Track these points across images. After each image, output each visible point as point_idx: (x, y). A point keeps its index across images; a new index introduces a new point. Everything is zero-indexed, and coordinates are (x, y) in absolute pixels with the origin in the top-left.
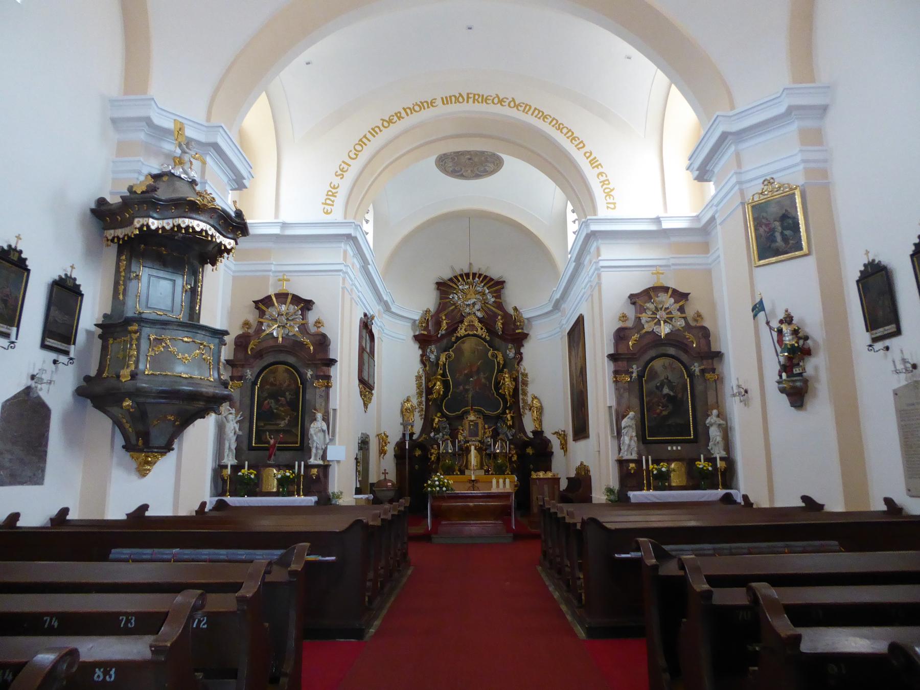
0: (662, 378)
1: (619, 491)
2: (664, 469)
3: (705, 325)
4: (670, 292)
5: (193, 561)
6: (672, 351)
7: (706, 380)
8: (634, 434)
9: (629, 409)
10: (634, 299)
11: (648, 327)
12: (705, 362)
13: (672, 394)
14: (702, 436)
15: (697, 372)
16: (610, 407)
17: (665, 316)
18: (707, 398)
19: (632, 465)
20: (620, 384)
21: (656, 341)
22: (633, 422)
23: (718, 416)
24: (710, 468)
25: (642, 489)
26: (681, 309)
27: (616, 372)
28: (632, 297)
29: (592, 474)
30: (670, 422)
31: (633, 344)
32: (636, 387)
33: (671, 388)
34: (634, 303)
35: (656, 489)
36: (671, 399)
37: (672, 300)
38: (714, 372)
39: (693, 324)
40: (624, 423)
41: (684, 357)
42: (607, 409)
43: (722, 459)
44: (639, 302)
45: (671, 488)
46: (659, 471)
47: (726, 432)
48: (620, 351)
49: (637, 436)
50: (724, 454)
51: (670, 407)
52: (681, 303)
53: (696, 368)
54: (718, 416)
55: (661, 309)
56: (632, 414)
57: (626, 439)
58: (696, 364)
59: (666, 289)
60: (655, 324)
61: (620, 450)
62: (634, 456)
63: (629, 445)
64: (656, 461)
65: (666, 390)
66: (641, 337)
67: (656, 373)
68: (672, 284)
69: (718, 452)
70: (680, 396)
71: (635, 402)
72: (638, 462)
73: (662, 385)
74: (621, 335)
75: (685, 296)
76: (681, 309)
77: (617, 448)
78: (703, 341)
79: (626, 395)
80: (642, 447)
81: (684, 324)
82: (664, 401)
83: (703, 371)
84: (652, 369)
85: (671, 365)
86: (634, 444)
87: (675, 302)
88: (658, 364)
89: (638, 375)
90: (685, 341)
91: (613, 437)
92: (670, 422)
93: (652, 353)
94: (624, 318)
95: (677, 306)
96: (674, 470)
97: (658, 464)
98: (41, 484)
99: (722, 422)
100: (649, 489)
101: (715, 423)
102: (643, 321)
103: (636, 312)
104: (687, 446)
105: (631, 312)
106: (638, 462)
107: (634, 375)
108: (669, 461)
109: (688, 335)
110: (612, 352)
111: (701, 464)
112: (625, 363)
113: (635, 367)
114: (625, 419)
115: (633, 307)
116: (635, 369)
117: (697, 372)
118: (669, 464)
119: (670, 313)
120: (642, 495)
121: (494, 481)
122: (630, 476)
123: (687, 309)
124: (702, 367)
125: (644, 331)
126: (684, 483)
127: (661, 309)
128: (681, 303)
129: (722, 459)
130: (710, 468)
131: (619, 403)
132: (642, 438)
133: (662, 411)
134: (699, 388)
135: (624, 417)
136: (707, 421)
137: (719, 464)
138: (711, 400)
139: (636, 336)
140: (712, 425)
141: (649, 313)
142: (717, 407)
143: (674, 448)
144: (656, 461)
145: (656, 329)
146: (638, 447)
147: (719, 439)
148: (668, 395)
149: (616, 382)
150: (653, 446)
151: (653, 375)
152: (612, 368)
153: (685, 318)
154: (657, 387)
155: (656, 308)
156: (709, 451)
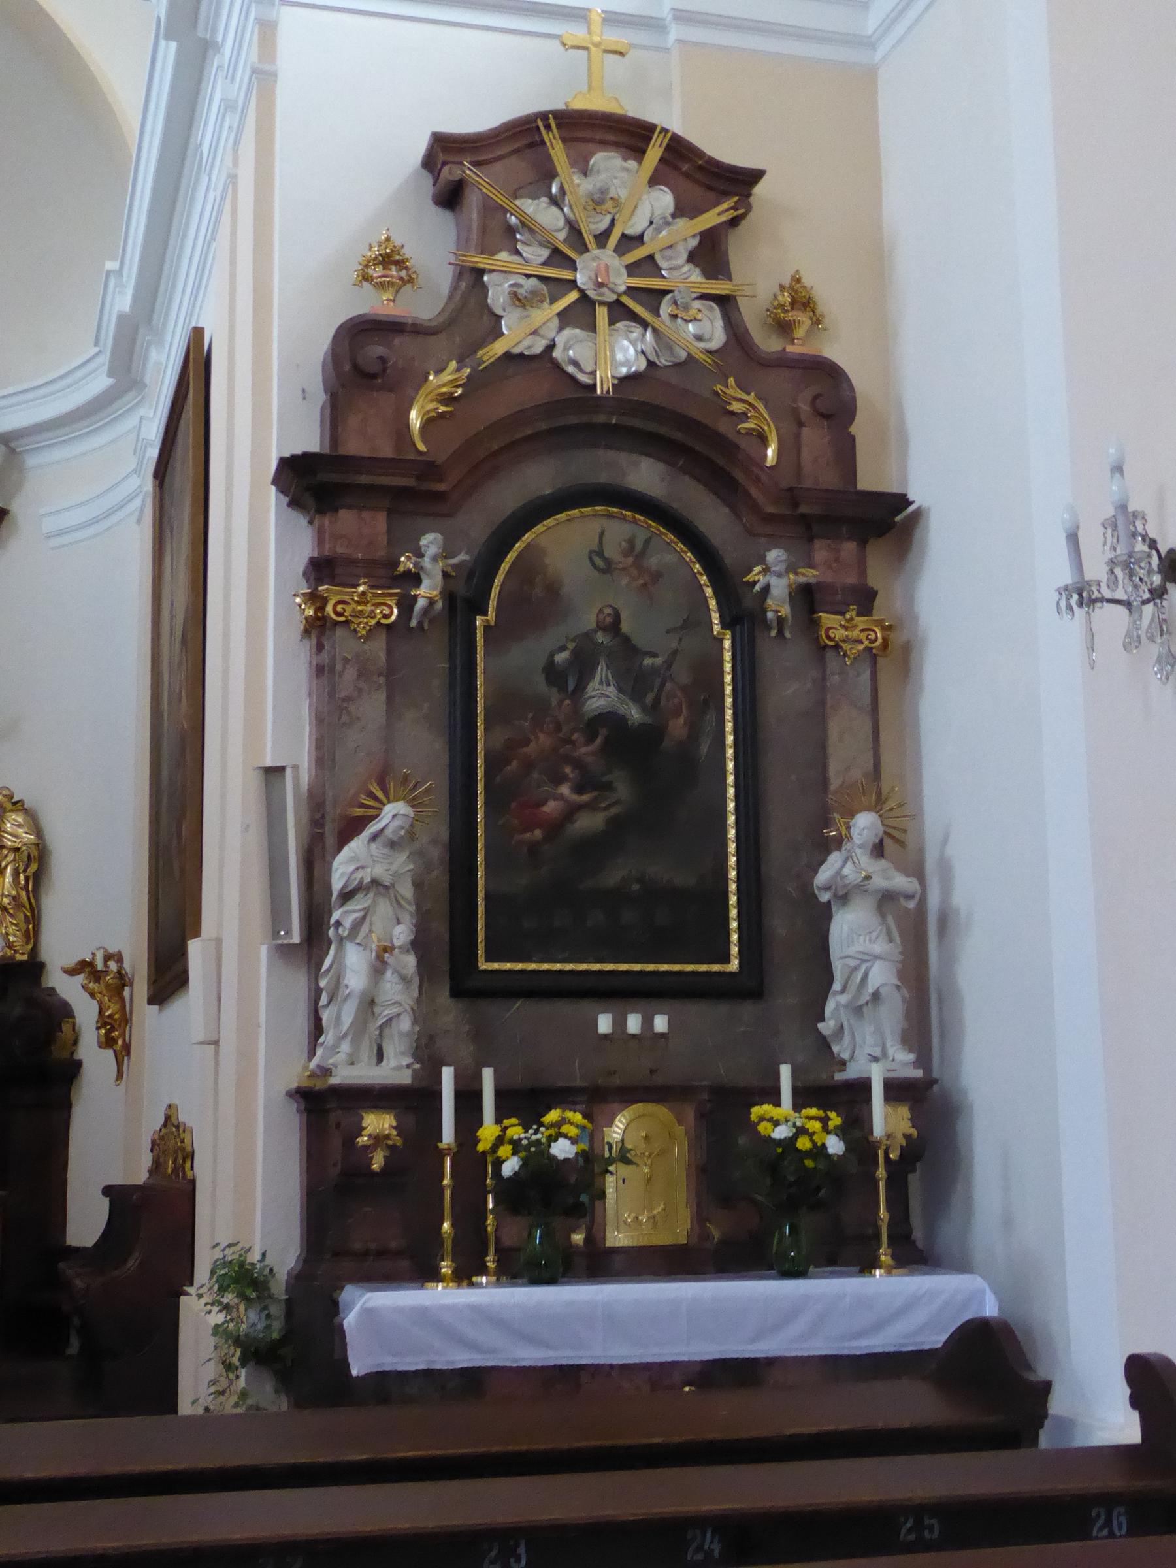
0: (589, 620)
1: (299, 1279)
2: (562, 1149)
3: (833, 352)
4: (654, 153)
6: (646, 475)
7: (822, 650)
8: (402, 934)
9: (386, 779)
10: (453, 167)
11: (518, 333)
12: (821, 551)
13: (634, 714)
14: (785, 965)
15: (779, 603)
16: (273, 773)
17: (622, 281)
18: (824, 768)
19: (378, 1123)
20: (343, 644)
21: (573, 415)
22: (402, 862)
23: (878, 850)
24: (835, 1146)
25: (427, 1274)
26: (710, 254)
27: (322, 569)
28: (444, 149)
29: (202, 1171)
30: (614, 875)
31: (429, 423)
32: (434, 657)
33: (635, 683)
34: (450, 197)
35: (516, 1268)
36: (625, 743)
37: (664, 199)
38: (866, 609)
39: (769, 344)
40: (346, 864)
41: (713, 518)
42: (256, 782)
43: (896, 1090)
44: (483, 183)
45: (599, 1264)
46: (539, 1164)
47: (919, 933)
48: (354, 447)
49: (418, 945)
50: (904, 1062)
51: (623, 790)
52: (712, 218)
53: (775, 577)
54: (878, 850)
55: (602, 239)
56: (394, 814)
57: (354, 965)
58: (774, 555)
59: (631, 135)
60: (565, 318)
61: (317, 1029)
62: (396, 1069)
63: (369, 1003)
64: (523, 1102)
65: (602, 694)
66: (471, 384)
67: (553, 590)
68: (671, 116)
69: (873, 1053)
70: (677, 727)
71: (423, 747)
72: (415, 1102)
74: (364, 361)
75: (737, 182)
76: (710, 254)
77: (301, 1024)
78: (815, 438)
79: (372, 707)
80: (451, 1014)
81: (717, 335)
82: (585, 751)
83: (808, 599)
84: (527, 569)
85: (636, 552)
86: (397, 994)
87: (683, 210)
88: (566, 544)
89: (450, 596)
90: (723, 426)
91: (284, 951)
92: (615, 874)
93: (538, 477)
94: (389, 261)
95: (688, 231)
96: (624, 1157)
97: (531, 1119)
99: (902, 882)
100: (464, 1275)
101: (861, 888)
102: (498, 293)
103: (463, 243)
104: (704, 1015)
105: (433, 247)
106: (415, 1102)
107: (427, 591)
108: (598, 1099)
109: (737, 397)
110: (308, 439)
111: (780, 1120)
112: (378, 523)
113: (430, 542)
114: (357, 846)
115: (444, 218)
116: (432, 557)
117: (779, 603)
118: (596, 1118)
119: (648, 265)
120: (422, 1315)
122: (374, 1193)
123: (737, 249)
124: (809, 575)
125: (498, 348)
126: (678, 1232)
127: (602, 239)
128: (712, 218)
129: (896, 1090)
130: (835, 1146)
131: (324, 756)
132: (451, 960)
133: (572, 811)
134: (785, 693)
135: (351, 828)
136: (824, 875)
137: (886, 1121)
138: (845, 758)
139: (446, 378)
140: (844, 899)
141: (535, 254)
142: (877, 804)
143: (634, 1024)
144: (523, 1102)
145: (572, 347)
146: (422, 1013)
147: (881, 976)
148: (610, 720)
149: (318, 627)
150: (517, 1014)
151: (536, 602)
152: (304, 544)
153: (725, 302)
155: (574, 229)
156: (824, 1044)
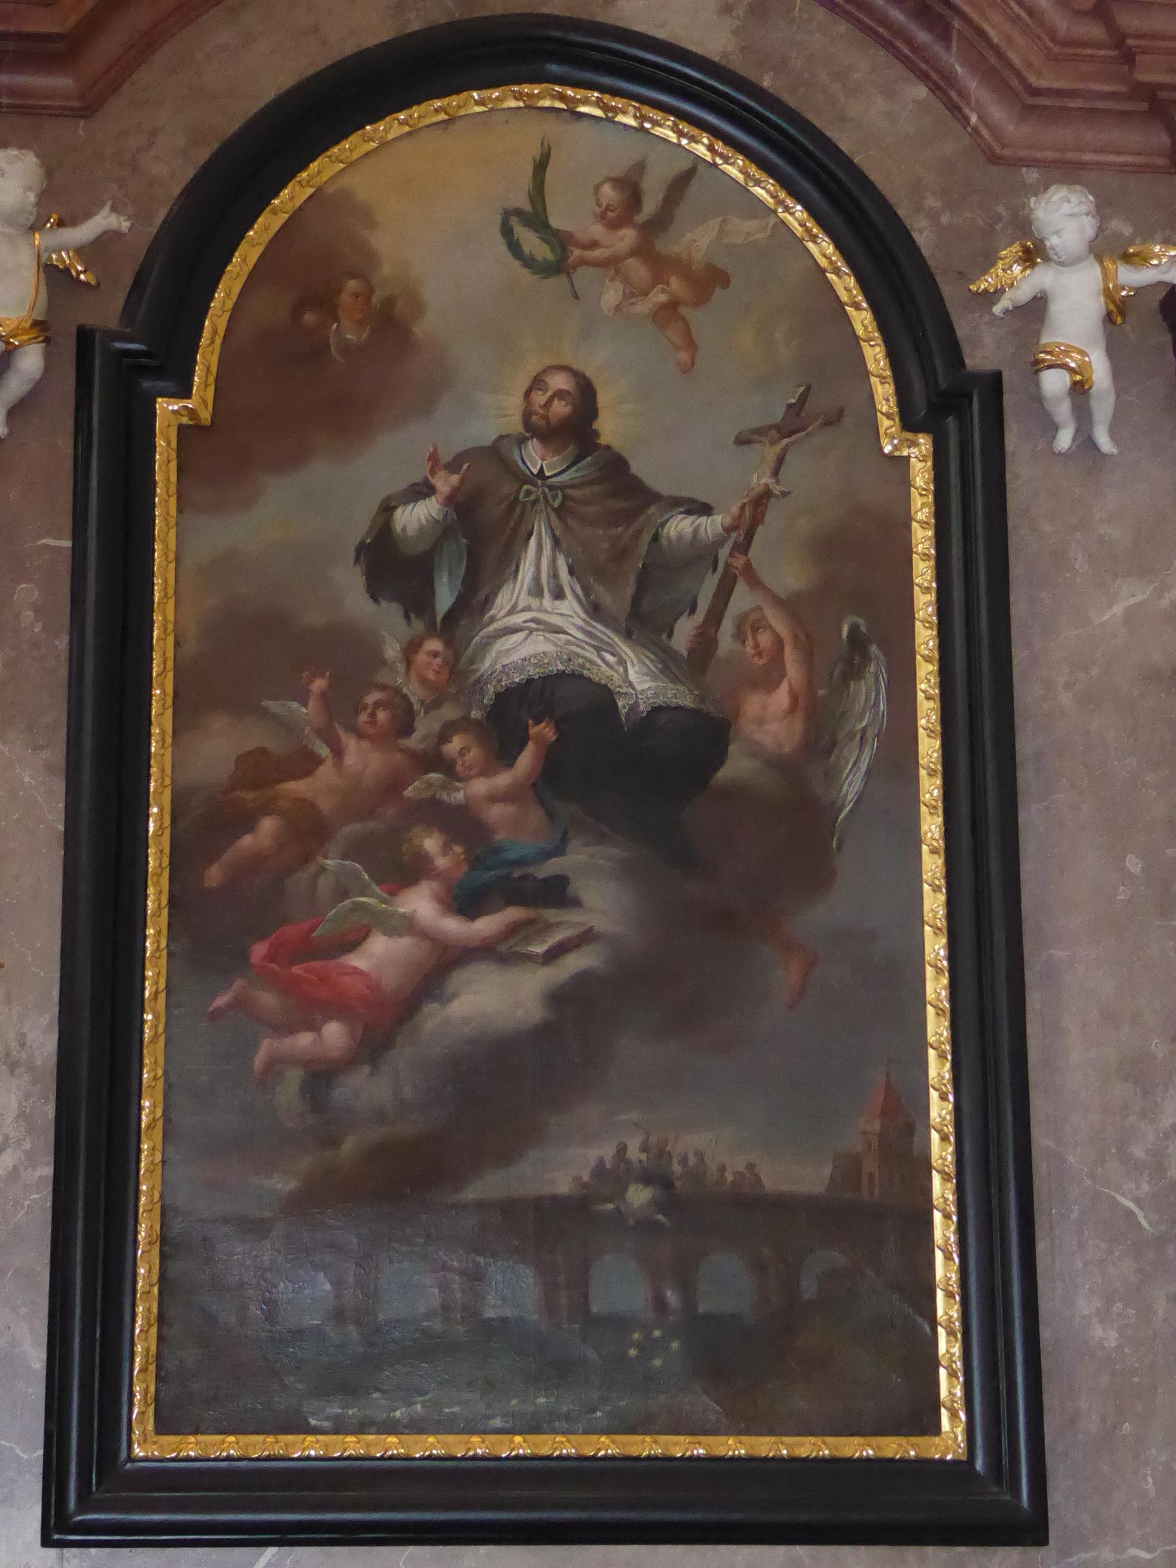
0: (494, 414)
5: (404, 1459)
13: (636, 679)
30: (562, 1166)
33: (643, 592)
36: (624, 770)
65: (539, 623)
67: (392, 324)
70: (769, 721)
73: (482, 533)
84: (317, 270)
98: (47, 1541)
121: (877, 1193)
133: (443, 964)
148: (559, 702)
154: (390, 566)
